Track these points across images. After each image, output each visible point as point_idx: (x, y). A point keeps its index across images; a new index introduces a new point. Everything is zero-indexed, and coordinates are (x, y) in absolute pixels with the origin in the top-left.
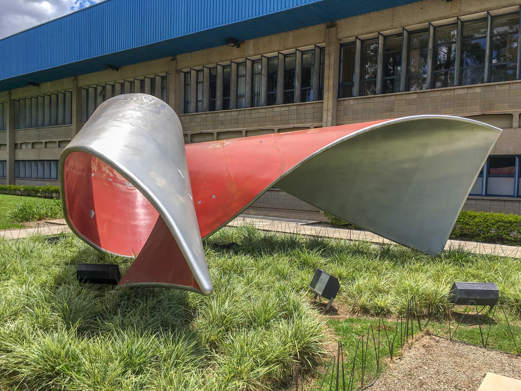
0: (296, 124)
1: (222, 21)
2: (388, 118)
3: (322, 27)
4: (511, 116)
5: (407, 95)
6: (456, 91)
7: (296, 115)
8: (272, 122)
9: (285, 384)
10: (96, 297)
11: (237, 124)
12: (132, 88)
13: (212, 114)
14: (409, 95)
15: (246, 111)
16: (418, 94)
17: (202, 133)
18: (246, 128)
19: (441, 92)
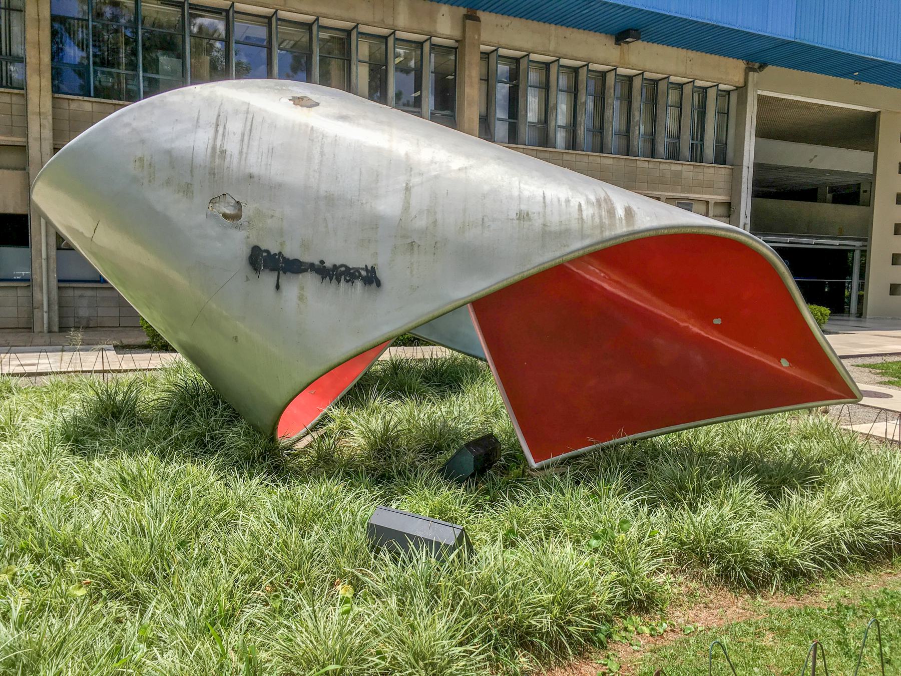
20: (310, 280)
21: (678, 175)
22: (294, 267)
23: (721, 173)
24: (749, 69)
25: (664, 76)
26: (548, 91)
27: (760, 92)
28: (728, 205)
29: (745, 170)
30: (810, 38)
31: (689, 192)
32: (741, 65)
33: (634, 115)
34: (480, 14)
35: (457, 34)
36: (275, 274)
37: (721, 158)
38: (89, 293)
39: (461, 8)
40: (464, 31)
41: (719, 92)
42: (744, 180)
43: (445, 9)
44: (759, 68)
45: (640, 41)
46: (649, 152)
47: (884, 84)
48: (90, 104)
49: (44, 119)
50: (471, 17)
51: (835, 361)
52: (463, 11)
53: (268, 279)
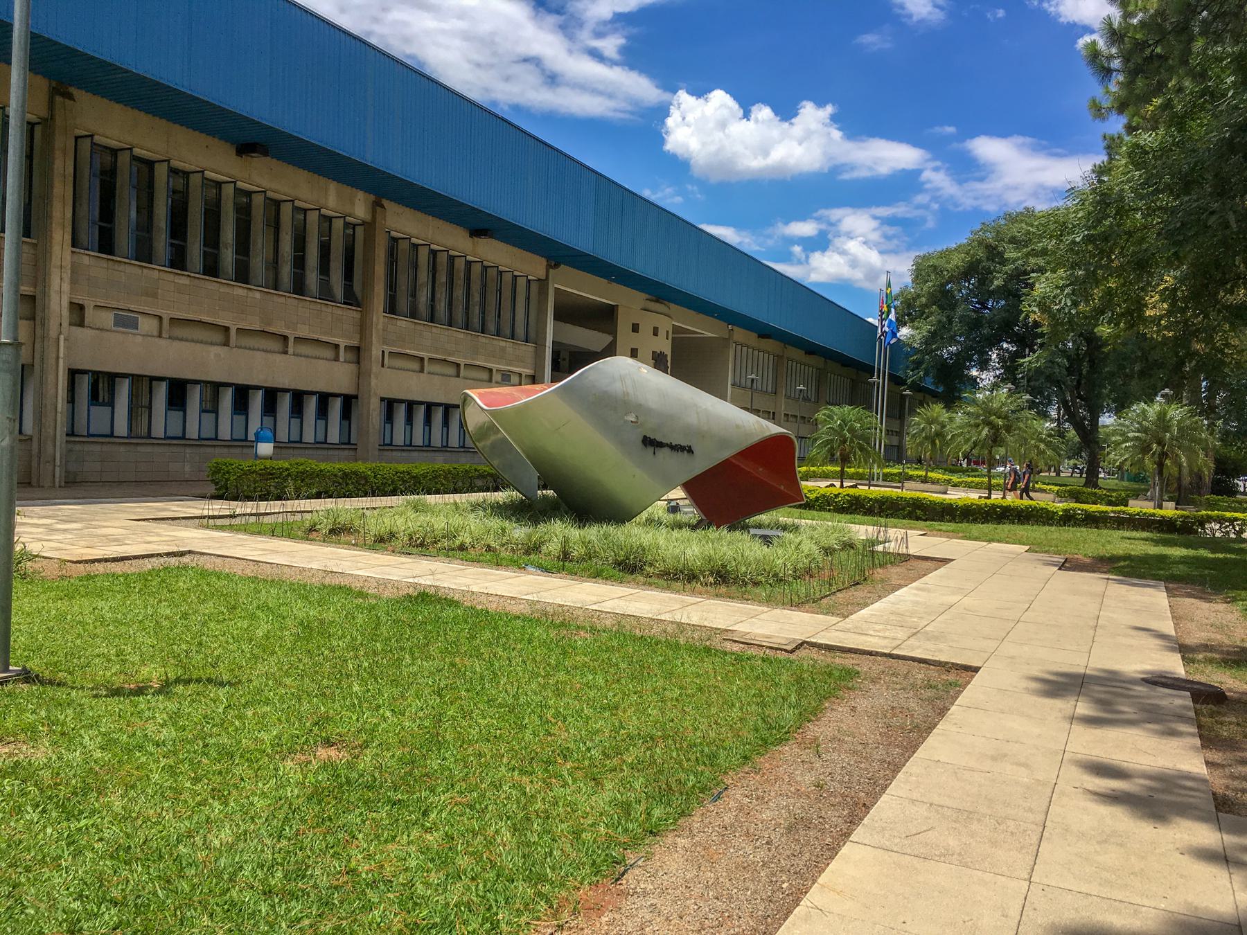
17: (445, 360)
20: (666, 450)
21: (503, 349)
22: (660, 445)
23: (528, 350)
24: (549, 267)
25: (87, 133)
26: (278, 229)
27: (556, 286)
28: (357, 350)
29: (547, 348)
30: (600, 253)
31: (510, 365)
32: (543, 261)
33: (473, 295)
34: (385, 202)
35: (368, 218)
36: (653, 448)
37: (350, 299)
38: (97, 448)
39: (372, 195)
40: (374, 217)
41: (205, 181)
42: (547, 358)
43: (360, 195)
44: (555, 265)
45: (269, 158)
46: (271, 283)
47: (578, 268)
48: (87, 258)
49: (64, 272)
50: (377, 204)
51: (689, 498)
52: (372, 197)
53: (651, 450)
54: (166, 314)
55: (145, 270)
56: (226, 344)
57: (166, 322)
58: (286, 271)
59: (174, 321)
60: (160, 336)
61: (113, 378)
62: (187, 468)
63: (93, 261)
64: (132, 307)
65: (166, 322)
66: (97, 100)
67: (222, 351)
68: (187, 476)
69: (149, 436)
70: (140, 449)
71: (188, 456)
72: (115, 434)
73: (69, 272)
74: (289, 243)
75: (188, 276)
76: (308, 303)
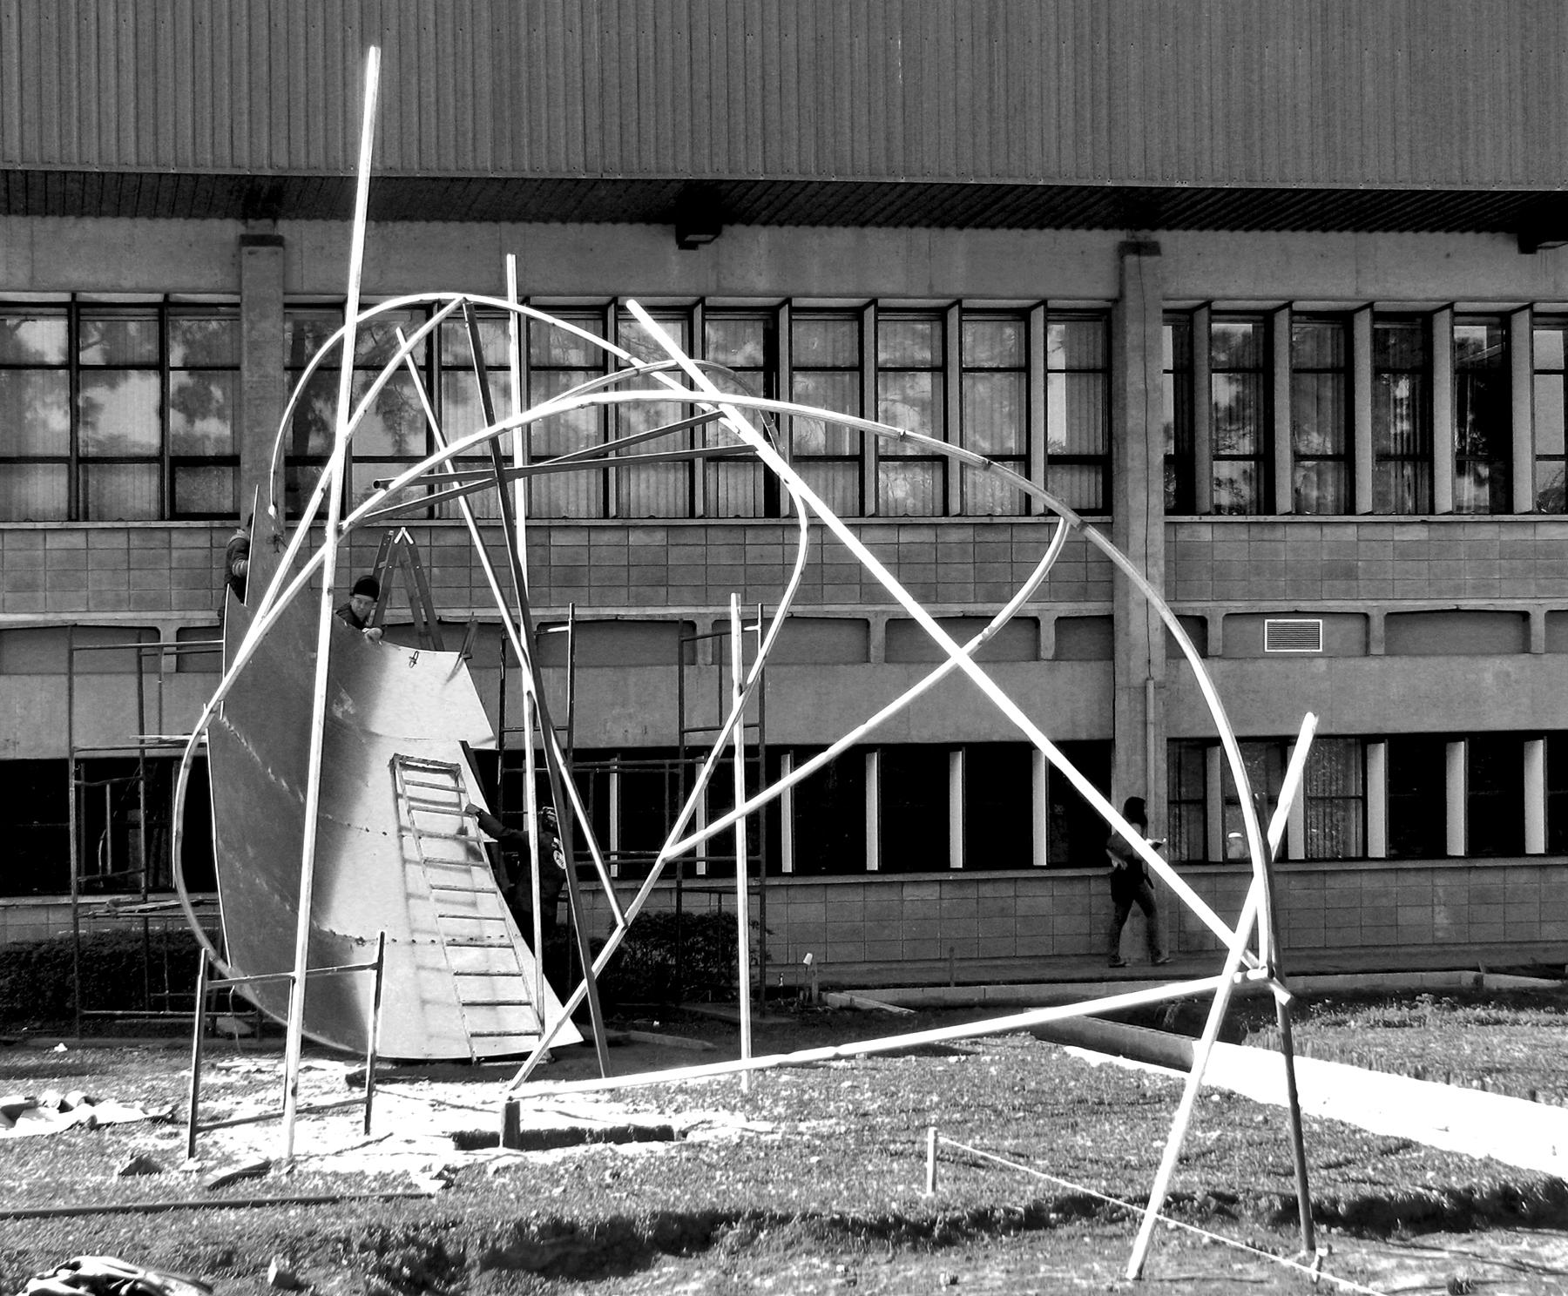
0: (975, 602)
1: (99, 81)
2: (287, 608)
3: (230, 229)
4: (1525, 616)
5: (1397, 529)
6: (1541, 528)
7: (971, 566)
8: (467, 590)
9: (416, 1284)
10: (1554, 1259)
11: (664, 589)
12: (1470, 319)
13: (622, 534)
14: (1404, 529)
15: (711, 532)
16: (1433, 526)
17: (1458, 610)
18: (711, 610)
19: (1496, 528)
54: (1377, 608)
55: (1327, 530)
56: (1525, 648)
57: (1378, 625)
58: (228, 523)
59: (1392, 617)
60: (1367, 653)
61: (1435, 744)
62: (1442, 918)
63: (1220, 533)
64: (1305, 606)
65: (1378, 625)
66: (1178, 234)
67: (1511, 665)
68: (1440, 934)
69: (1365, 857)
70: (1330, 882)
71: (1441, 892)
72: (1371, 855)
73: (1162, 563)
74: (1449, 391)
75: (1423, 522)
76: (1244, 529)
